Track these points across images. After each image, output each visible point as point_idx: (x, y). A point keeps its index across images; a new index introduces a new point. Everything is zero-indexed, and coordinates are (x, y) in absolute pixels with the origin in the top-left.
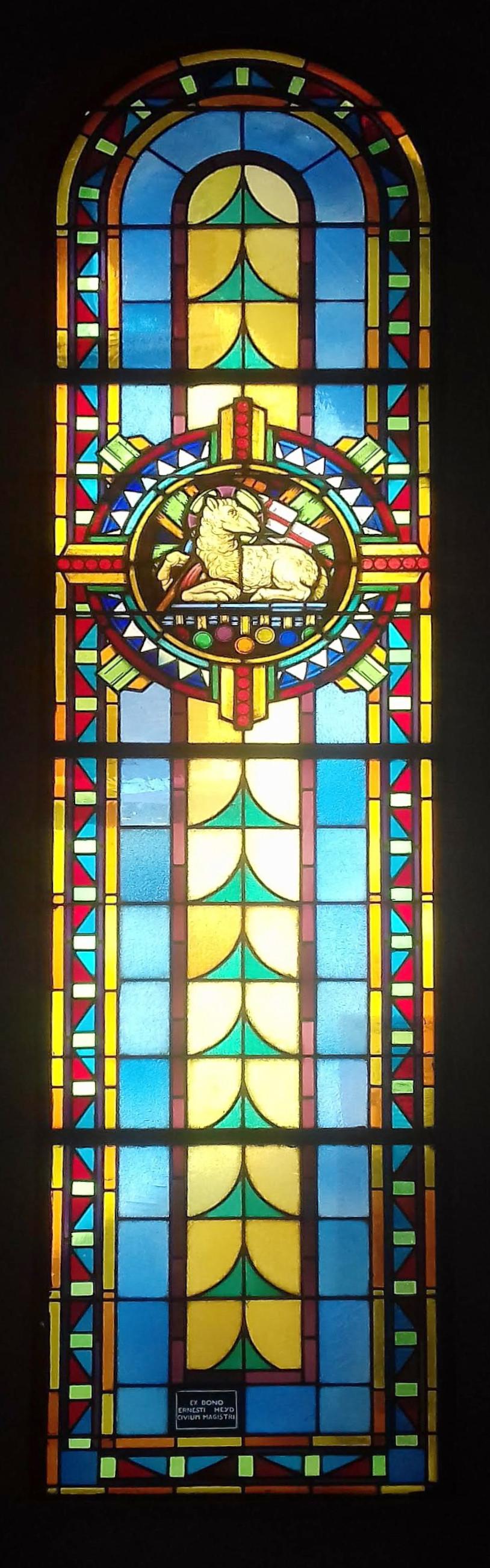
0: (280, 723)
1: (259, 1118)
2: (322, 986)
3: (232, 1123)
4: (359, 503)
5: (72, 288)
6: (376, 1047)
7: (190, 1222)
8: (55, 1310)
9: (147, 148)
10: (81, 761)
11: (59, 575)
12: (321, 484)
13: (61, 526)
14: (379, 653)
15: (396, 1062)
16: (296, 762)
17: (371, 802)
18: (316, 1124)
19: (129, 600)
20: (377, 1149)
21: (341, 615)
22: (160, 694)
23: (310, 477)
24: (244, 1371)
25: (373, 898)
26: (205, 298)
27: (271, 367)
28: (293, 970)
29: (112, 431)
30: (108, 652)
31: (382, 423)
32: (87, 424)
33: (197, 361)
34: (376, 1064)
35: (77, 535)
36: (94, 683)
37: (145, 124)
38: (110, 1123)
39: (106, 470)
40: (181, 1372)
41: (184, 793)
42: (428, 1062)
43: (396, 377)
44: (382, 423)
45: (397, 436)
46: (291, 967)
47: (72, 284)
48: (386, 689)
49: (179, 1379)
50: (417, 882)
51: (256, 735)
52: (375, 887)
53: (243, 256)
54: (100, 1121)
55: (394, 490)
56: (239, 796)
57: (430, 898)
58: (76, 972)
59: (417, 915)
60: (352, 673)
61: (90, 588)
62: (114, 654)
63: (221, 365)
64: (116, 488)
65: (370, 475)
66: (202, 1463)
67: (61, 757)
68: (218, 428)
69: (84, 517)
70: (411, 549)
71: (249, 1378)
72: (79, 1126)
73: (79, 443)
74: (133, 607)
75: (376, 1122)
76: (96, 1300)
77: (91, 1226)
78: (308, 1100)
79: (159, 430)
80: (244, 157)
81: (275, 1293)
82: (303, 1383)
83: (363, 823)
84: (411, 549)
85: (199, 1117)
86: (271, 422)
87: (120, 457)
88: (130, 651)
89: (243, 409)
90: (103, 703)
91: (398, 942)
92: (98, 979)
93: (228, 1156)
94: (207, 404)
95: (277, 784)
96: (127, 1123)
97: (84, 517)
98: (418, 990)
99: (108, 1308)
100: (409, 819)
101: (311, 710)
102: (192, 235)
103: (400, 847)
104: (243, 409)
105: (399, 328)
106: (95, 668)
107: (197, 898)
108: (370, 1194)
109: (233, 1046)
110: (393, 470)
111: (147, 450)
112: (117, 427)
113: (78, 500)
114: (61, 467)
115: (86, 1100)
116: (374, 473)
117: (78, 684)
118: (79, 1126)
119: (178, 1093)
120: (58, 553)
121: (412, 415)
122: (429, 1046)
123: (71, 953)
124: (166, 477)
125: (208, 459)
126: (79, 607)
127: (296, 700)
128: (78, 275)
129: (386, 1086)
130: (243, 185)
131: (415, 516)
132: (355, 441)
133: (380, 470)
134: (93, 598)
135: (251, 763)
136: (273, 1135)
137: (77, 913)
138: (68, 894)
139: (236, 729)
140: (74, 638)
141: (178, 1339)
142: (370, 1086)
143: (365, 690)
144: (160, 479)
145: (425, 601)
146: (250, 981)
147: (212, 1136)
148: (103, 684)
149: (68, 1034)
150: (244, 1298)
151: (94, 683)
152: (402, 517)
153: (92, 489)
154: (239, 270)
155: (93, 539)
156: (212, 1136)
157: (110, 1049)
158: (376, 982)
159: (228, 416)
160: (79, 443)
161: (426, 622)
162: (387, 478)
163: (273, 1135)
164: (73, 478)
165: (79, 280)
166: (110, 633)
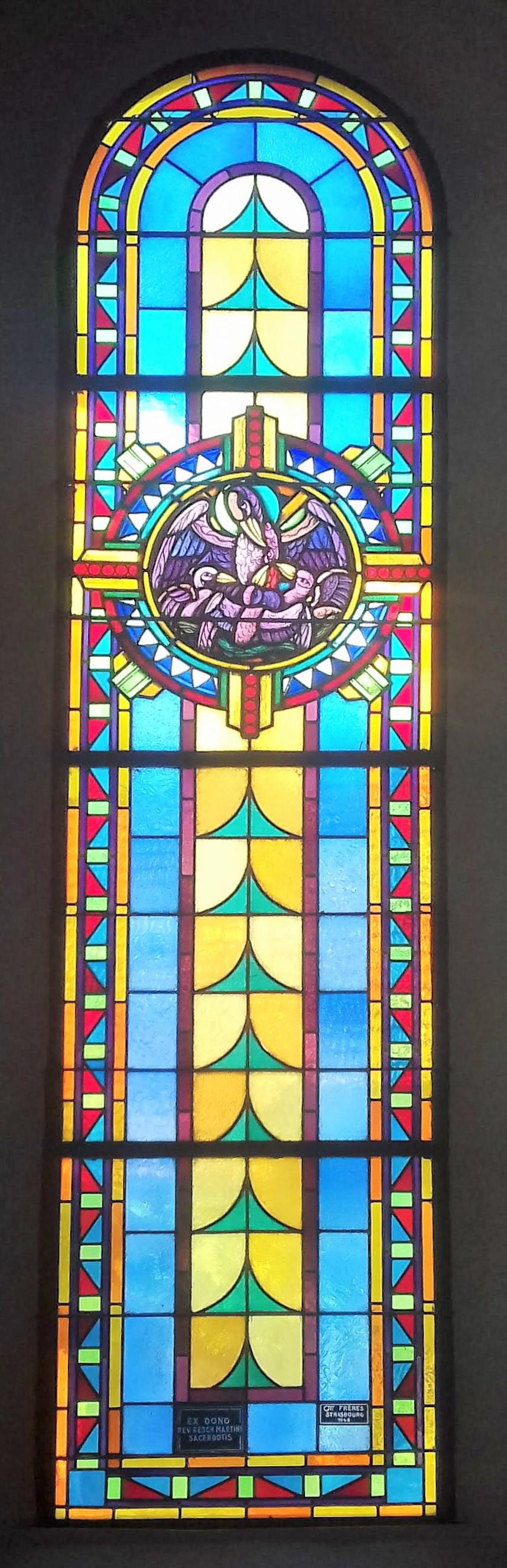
0: (285, 731)
1: (261, 1131)
2: (321, 1235)
3: (238, 1136)
4: (367, 514)
5: (85, 665)
6: (376, 1061)
7: (198, 919)
8: (71, 926)
9: (165, 158)
10: (102, 394)
11: (75, 580)
12: (331, 493)
13: (79, 532)
14: (381, 663)
15: (395, 1075)
16: (306, 396)
17: (372, 715)
18: (318, 1137)
19: (142, 605)
20: (375, 774)
21: (347, 623)
22: (170, 701)
23: (318, 485)
24: (246, 1388)
25: (373, 909)
26: (215, 989)
27: (281, 374)
28: (297, 828)
29: (130, 438)
30: (121, 660)
31: (387, 434)
32: (106, 430)
33: (211, 367)
34: (376, 1077)
35: (96, 541)
36: (106, 688)
37: (161, 137)
38: (124, 746)
39: (123, 477)
40: (186, 1391)
41: (191, 803)
42: (426, 1077)
43: (400, 1149)
44: (387, 434)
45: (399, 445)
46: (295, 826)
47: (73, 1357)
48: (388, 699)
49: (183, 1397)
50: (416, 702)
51: (264, 743)
52: (375, 898)
53: (249, 794)
54: (114, 744)
55: (398, 498)
56: (243, 1362)
57: (428, 909)
58: (89, 886)
59: (416, 642)
60: (354, 682)
61: (108, 594)
62: (125, 662)
63: (228, 1138)
64: (131, 496)
65: (374, 484)
66: (202, 1483)
67: (74, 765)
68: (232, 435)
69: (101, 523)
70: (413, 559)
71: (251, 1395)
72: (93, 749)
73: (98, 449)
74: (147, 614)
75: (377, 1135)
76: (104, 1316)
77: (104, 941)
78: (311, 1110)
79: (175, 439)
80: (256, 168)
81: (277, 1065)
82: (304, 1401)
83: (364, 834)
84: (413, 559)
85: (207, 1130)
86: (282, 430)
87: (135, 465)
88: (141, 658)
89: (250, 727)
90: (116, 710)
91: (396, 953)
92: (108, 990)
93: (233, 778)
94: (222, 412)
95: (282, 791)
96: (146, 370)
97: (101, 523)
98: (417, 527)
99: (115, 1324)
100: (408, 829)
101: (314, 1108)
102: (195, 1321)
103: (400, 857)
104: (255, 418)
105: (402, 1100)
106: (108, 674)
107: (202, 1065)
108: (369, 1106)
109: (239, 826)
110: (397, 479)
111: (164, 459)
112: (134, 435)
113: (96, 507)
114: (80, 474)
115: (108, 349)
116: (377, 481)
117: (92, 692)
118: (93, 749)
119: (185, 1104)
120: (75, 558)
121: (416, 423)
122: (426, 1061)
123: (94, 301)
124: (183, 484)
125: (222, 467)
126: (95, 613)
127: (300, 709)
128: (79, 1346)
129: (385, 1101)
130: (256, 195)
131: (418, 527)
132: (359, 451)
133: (384, 479)
134: (108, 603)
135: (257, 772)
136: (275, 1148)
137: (88, 922)
138: (74, 1304)
139: (243, 737)
140: (84, 935)
141: (185, 1111)
142: (370, 1100)
143: (367, 700)
144: (177, 485)
145: (426, 612)
146: (253, 1232)
147: (226, 383)
148: (116, 690)
149: (85, 658)
150: (248, 1070)
151: (106, 688)
152: (405, 527)
153: (108, 494)
154: (243, 1200)
155: (107, 545)
156: (220, 1149)
157: (119, 1063)
158: (375, 994)
159: (240, 426)
160: (98, 449)
161: (426, 631)
162: (391, 486)
163: (275, 1148)
164: (91, 483)
165: (96, 472)
166: (127, 644)
